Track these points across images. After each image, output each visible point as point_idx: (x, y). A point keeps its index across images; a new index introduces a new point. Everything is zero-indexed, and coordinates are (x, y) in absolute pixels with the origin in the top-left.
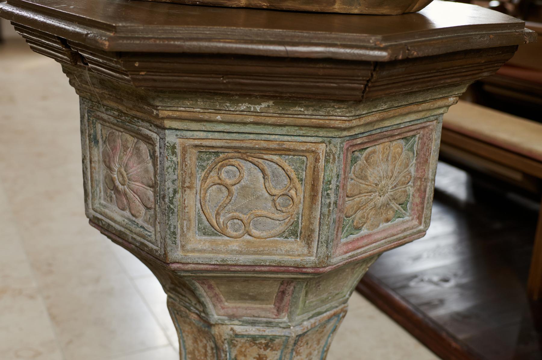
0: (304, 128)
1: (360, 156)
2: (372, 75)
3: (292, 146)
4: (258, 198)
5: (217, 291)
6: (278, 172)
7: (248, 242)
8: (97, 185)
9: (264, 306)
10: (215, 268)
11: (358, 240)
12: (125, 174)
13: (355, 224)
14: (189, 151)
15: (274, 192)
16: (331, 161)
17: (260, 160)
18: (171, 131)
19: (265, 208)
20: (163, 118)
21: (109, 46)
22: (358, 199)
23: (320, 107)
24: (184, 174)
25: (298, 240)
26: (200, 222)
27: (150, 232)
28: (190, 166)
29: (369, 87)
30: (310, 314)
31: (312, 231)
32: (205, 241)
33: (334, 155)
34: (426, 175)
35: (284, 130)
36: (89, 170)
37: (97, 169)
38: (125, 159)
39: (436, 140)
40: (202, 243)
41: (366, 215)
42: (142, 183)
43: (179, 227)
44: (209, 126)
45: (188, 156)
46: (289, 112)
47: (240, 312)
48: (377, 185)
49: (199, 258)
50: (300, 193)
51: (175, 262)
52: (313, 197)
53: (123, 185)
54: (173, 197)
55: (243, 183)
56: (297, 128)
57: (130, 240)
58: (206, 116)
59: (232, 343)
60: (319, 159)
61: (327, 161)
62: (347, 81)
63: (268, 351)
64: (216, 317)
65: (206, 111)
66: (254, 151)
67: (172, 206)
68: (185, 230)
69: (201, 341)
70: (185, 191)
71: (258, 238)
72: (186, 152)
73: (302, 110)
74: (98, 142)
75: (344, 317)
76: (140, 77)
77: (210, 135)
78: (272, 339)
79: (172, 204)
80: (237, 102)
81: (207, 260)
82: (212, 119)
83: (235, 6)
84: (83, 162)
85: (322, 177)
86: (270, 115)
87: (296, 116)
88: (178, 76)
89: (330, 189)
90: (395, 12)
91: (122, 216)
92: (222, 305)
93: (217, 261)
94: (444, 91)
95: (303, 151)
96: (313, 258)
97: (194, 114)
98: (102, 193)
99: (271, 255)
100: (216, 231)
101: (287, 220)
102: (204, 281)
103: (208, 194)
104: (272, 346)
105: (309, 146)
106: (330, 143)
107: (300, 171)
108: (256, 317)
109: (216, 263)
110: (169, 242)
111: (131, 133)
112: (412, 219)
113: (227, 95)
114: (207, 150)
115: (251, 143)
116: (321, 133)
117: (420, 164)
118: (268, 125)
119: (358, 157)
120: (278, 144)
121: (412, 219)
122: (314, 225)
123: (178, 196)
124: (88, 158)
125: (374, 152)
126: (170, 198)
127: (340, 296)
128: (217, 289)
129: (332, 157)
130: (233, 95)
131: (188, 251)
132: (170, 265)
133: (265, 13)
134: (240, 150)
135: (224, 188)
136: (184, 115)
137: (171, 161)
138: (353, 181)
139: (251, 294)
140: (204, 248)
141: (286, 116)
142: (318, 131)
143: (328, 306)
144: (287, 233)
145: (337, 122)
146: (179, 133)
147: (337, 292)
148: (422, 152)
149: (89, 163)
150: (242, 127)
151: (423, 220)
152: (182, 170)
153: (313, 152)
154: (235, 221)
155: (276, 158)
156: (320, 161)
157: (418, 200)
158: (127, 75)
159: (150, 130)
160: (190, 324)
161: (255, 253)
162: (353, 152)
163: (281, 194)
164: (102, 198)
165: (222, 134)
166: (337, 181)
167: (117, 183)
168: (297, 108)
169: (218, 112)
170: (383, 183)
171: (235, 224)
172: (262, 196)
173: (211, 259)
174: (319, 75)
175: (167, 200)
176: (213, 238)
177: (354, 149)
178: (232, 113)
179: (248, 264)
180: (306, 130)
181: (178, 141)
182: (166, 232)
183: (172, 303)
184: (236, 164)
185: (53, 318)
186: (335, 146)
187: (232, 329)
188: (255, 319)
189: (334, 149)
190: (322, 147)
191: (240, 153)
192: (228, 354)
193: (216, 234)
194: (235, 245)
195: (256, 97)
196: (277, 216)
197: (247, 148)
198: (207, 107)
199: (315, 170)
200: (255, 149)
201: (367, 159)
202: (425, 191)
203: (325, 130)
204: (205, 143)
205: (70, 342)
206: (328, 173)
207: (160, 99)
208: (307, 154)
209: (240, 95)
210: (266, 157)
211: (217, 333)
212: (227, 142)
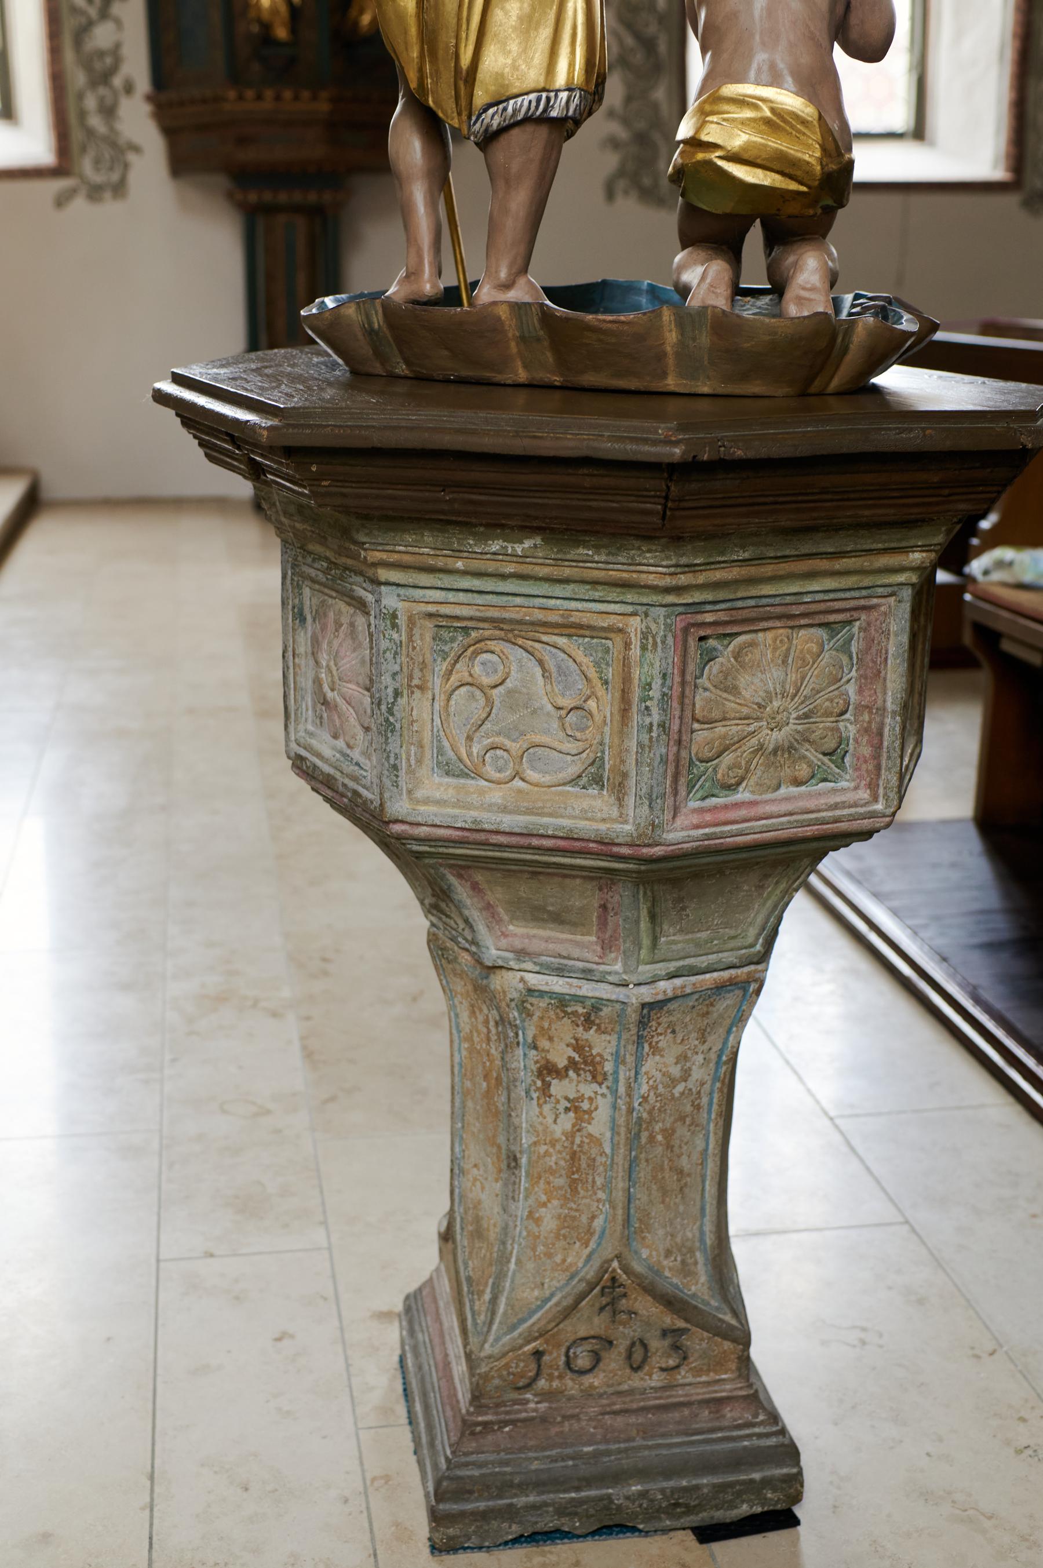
0: (600, 588)
1: (720, 647)
2: (668, 488)
3: (585, 619)
4: (534, 712)
5: (490, 897)
6: (568, 668)
7: (520, 791)
8: (303, 698)
9: (579, 938)
10: (464, 837)
11: (726, 807)
12: (334, 668)
13: (719, 776)
14: (418, 625)
15: (561, 702)
16: (649, 647)
17: (537, 645)
18: (390, 588)
19: (547, 732)
20: (375, 565)
21: (268, 437)
22: (723, 730)
23: (619, 549)
24: (411, 663)
25: (605, 792)
26: (441, 751)
27: (366, 771)
28: (421, 650)
29: (671, 509)
30: (672, 966)
31: (625, 775)
32: (448, 785)
33: (654, 637)
34: (880, 702)
35: (568, 590)
36: (291, 670)
37: (303, 669)
38: (336, 643)
39: (896, 635)
40: (442, 789)
41: (743, 763)
42: (358, 684)
43: (404, 756)
44: (447, 581)
45: (416, 631)
46: (568, 557)
47: (536, 946)
48: (759, 706)
49: (436, 815)
50: (603, 706)
51: (397, 821)
52: (625, 712)
53: (332, 690)
54: (393, 703)
55: (509, 684)
56: (588, 587)
57: (341, 789)
58: (440, 563)
59: (522, 1006)
60: (631, 643)
61: (644, 648)
62: (633, 498)
63: (592, 1032)
64: (494, 952)
65: (438, 552)
66: (524, 627)
67: (391, 719)
68: (413, 762)
69: (481, 1010)
70: (413, 692)
71: (536, 785)
72: (414, 624)
73: (590, 553)
74: (305, 619)
75: (758, 992)
76: (323, 490)
77: (451, 596)
78: (597, 1005)
79: (392, 714)
80: (484, 538)
81: (449, 820)
82: (450, 567)
83: (509, 382)
84: (284, 657)
85: (637, 677)
86: (540, 561)
87: (581, 564)
88: (379, 489)
89: (651, 699)
90: (780, 392)
91: (334, 748)
92: (504, 929)
93: (465, 821)
94: (884, 537)
95: (603, 629)
96: (628, 827)
97: (421, 557)
98: (310, 712)
99: (556, 817)
100: (466, 770)
101: (584, 755)
102: (463, 872)
103: (452, 702)
104: (597, 1021)
105: (612, 620)
106: (646, 615)
107: (603, 666)
108: (564, 958)
109: (463, 825)
110: (387, 783)
111: (346, 599)
112: (856, 788)
113: (466, 524)
114: (449, 624)
115: (518, 612)
116: (629, 597)
117: (866, 678)
118: (541, 579)
119: (715, 649)
120: (562, 616)
121: (856, 788)
122: (627, 764)
123: (402, 701)
124: (290, 649)
125: (752, 644)
126: (388, 704)
127: (738, 943)
128: (489, 893)
129: (650, 640)
130: (476, 526)
131: (418, 802)
132: (391, 826)
133: (557, 395)
134: (502, 626)
135: (478, 693)
136: (407, 559)
137: (390, 640)
138: (707, 694)
139: (550, 908)
140: (445, 798)
141: (567, 563)
142: (624, 593)
143: (713, 958)
144: (584, 780)
145: (651, 577)
146: (402, 591)
147: (732, 932)
148: (869, 657)
149: (291, 657)
150: (500, 583)
151: (881, 791)
152: (408, 655)
153: (620, 631)
154: (499, 752)
155: (562, 641)
156: (633, 647)
157: (866, 751)
158: (305, 487)
159: (364, 589)
160: (461, 975)
161: (529, 812)
162: (702, 639)
163: (572, 706)
164: (310, 720)
165: (470, 595)
166: (663, 685)
167: (326, 688)
168: (582, 551)
169: (457, 554)
170: (776, 704)
171: (497, 758)
172: (541, 709)
173: (455, 817)
174: (586, 488)
175: (384, 707)
176: (462, 781)
177: (702, 633)
178: (479, 556)
179: (517, 830)
180: (604, 590)
181: (400, 605)
182: (383, 765)
183: (434, 935)
184: (497, 649)
185: (308, 1054)
186: (655, 621)
187: (522, 980)
188: (563, 961)
189: (653, 627)
190: (635, 622)
191: (502, 629)
192: (520, 1033)
193: (467, 774)
194: (496, 796)
195: (512, 528)
196: (571, 747)
197: (511, 621)
198: (439, 545)
199: (626, 663)
200: (526, 624)
201: (737, 655)
202: (880, 734)
203: (634, 590)
204: (445, 610)
205: (333, 1099)
206: (646, 670)
207: (367, 531)
208: (612, 635)
209: (487, 526)
210: (545, 638)
211: (499, 987)
212: (479, 610)
